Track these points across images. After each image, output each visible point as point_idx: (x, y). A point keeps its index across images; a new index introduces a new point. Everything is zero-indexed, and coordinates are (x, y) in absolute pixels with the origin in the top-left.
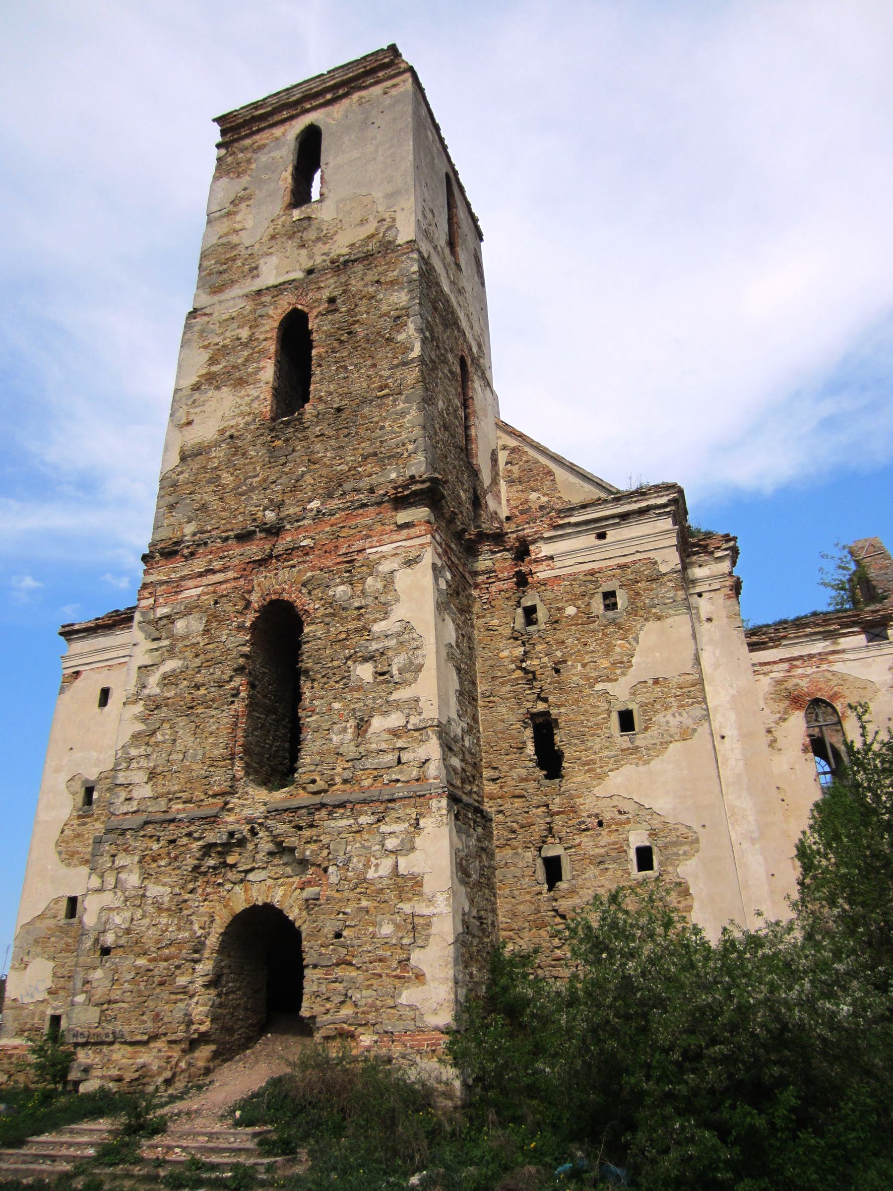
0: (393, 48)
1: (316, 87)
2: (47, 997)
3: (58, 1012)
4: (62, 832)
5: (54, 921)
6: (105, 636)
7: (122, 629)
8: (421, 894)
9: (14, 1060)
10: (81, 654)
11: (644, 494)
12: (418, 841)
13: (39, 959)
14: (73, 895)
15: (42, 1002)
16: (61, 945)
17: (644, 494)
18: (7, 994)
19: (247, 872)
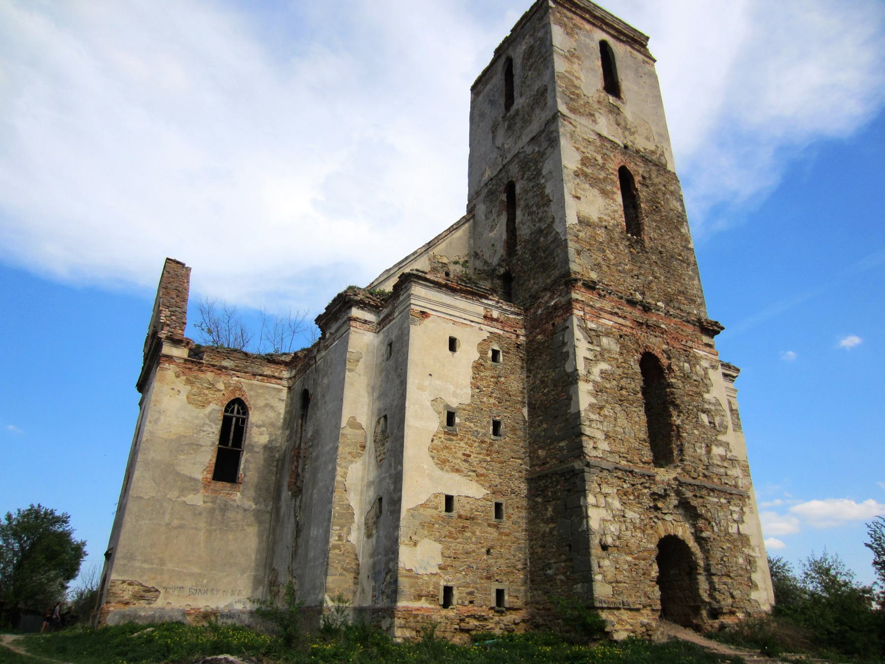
0: (648, 38)
1: (609, 20)
2: (439, 571)
3: (450, 584)
4: (432, 441)
5: (436, 512)
6: (446, 294)
7: (462, 297)
8: (750, 546)
9: (419, 618)
10: (425, 298)
11: (730, 368)
12: (745, 518)
13: (426, 540)
14: (450, 494)
15: (435, 575)
16: (445, 532)
17: (730, 368)
18: (401, 565)
19: (665, 514)
